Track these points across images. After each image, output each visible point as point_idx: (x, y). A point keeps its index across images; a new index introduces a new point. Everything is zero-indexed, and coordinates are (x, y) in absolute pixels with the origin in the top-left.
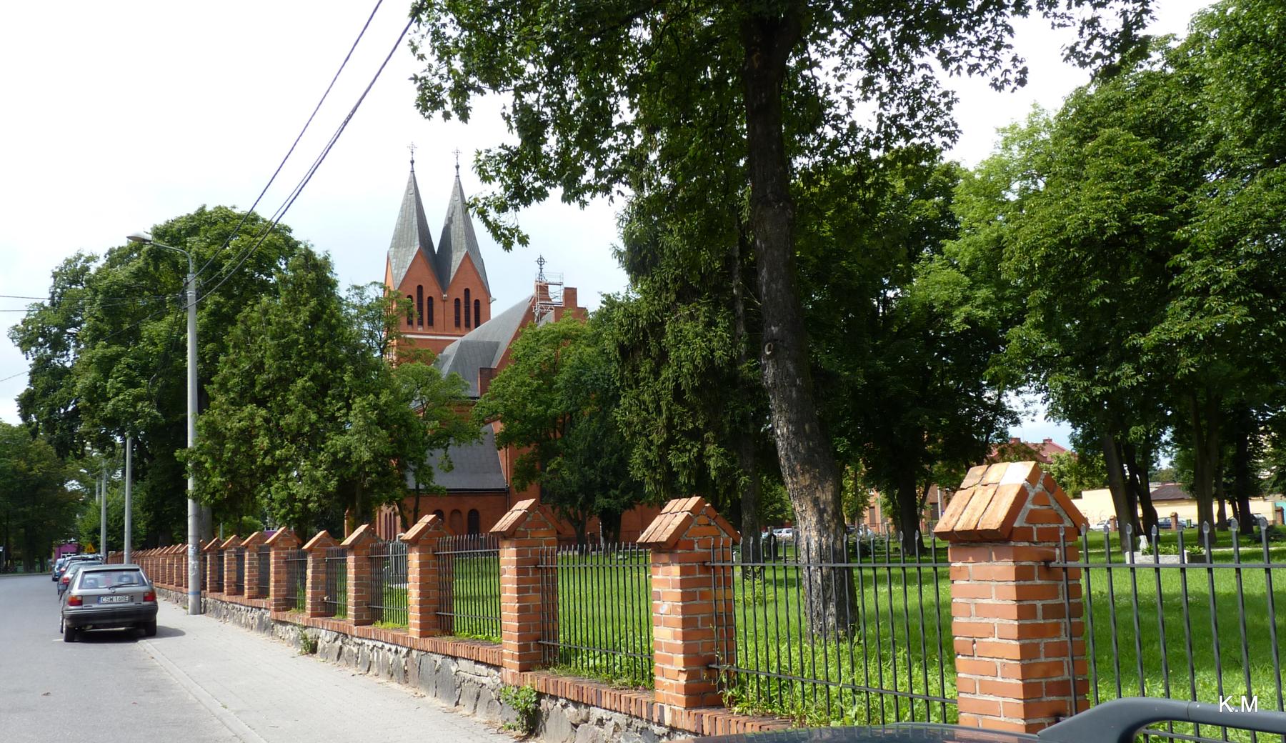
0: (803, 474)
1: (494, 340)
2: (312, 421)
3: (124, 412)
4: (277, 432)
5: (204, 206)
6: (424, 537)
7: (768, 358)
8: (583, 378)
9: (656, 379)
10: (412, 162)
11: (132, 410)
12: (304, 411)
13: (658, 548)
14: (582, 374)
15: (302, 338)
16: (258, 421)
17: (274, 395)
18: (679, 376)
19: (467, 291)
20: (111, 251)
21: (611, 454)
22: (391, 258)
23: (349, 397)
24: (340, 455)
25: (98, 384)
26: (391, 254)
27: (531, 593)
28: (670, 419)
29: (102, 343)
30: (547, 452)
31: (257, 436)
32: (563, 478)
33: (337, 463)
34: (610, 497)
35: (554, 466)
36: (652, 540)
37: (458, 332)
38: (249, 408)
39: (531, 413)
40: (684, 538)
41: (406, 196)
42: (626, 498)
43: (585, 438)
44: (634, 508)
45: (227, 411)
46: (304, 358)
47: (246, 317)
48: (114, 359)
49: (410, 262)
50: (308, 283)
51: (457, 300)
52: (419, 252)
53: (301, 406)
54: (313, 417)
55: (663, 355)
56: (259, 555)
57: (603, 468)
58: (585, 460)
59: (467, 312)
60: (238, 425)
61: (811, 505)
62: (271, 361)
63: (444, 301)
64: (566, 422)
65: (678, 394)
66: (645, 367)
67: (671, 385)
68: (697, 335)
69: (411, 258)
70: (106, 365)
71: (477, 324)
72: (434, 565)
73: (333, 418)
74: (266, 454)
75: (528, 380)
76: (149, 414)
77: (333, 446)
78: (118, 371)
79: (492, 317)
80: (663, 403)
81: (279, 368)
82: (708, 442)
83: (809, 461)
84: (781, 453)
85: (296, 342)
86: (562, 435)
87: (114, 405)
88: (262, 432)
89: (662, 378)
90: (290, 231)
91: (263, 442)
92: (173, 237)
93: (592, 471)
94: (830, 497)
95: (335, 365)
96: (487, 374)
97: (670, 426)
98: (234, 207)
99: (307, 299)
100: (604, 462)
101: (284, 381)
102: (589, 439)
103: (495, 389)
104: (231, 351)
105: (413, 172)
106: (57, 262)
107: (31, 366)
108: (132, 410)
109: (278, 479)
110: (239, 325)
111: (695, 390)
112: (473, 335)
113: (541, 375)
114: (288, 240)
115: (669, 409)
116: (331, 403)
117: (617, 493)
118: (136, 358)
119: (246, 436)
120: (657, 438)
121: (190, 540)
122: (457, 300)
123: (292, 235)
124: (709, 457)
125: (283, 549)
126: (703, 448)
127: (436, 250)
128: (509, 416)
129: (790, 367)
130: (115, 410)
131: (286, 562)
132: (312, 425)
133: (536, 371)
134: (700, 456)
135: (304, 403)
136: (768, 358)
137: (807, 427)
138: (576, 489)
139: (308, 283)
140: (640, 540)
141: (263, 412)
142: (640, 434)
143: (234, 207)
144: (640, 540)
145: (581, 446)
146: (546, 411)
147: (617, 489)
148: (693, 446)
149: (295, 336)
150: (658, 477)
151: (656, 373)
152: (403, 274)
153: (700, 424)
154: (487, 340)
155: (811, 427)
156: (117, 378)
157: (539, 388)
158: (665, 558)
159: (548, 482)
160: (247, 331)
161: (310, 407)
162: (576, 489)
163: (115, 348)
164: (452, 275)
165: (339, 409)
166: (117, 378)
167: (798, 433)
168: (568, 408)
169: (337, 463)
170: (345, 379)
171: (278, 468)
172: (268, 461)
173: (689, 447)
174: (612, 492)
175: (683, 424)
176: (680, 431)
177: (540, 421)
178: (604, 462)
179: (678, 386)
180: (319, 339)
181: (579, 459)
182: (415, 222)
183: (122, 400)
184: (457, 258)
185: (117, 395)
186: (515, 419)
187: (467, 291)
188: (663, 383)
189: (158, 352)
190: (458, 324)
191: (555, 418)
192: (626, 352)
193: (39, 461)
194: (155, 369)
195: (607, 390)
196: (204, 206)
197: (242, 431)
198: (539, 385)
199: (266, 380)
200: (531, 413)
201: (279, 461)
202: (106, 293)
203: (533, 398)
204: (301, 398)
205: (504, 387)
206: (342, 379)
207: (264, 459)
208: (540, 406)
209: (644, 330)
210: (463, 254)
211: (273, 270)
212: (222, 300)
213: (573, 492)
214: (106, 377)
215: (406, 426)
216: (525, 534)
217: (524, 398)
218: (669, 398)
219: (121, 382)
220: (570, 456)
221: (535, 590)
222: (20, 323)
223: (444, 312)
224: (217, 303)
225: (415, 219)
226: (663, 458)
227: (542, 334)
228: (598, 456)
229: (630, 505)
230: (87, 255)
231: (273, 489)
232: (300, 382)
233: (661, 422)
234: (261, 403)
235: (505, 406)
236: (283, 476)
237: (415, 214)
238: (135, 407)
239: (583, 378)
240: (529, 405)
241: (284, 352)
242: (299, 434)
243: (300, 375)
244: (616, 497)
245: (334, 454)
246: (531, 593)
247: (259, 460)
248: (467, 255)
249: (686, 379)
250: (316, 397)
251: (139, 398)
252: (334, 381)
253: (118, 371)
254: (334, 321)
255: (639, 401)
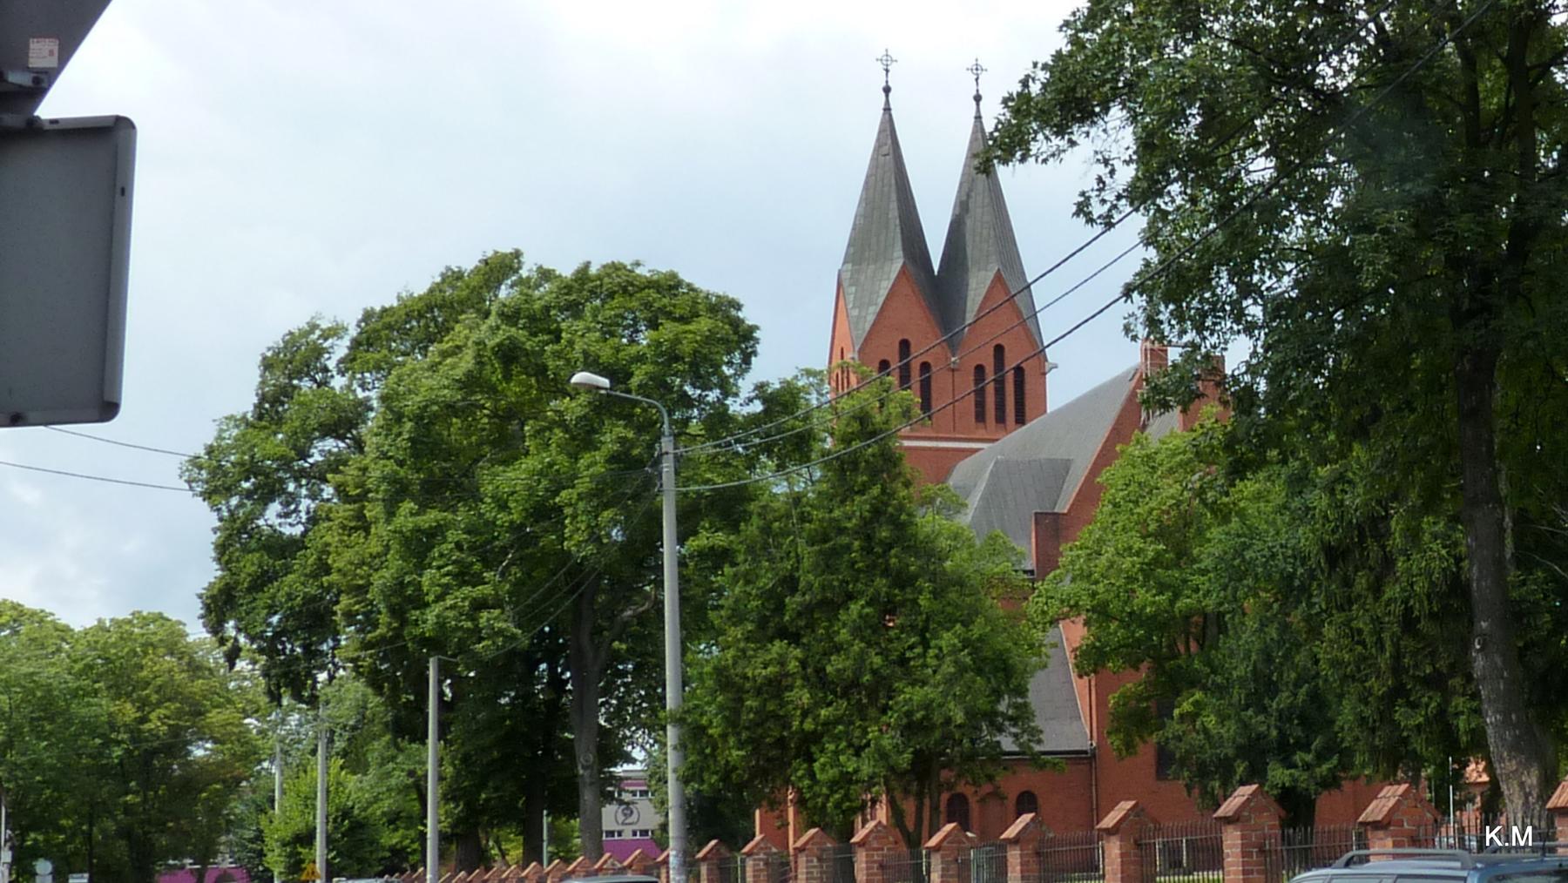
0: (1510, 760)
1: (1061, 454)
2: (875, 666)
3: (457, 628)
4: (819, 681)
5: (587, 265)
6: (1124, 825)
7: (1478, 651)
8: (1248, 555)
9: (1377, 599)
10: (887, 90)
11: (469, 624)
12: (862, 650)
13: (1377, 825)
14: (1246, 547)
15: (856, 544)
16: (793, 666)
17: (811, 627)
18: (1410, 597)
19: (999, 350)
20: (368, 316)
21: (1297, 685)
22: (845, 284)
23: (925, 629)
24: (919, 715)
25: (407, 579)
26: (846, 276)
27: (1255, 875)
28: (1397, 656)
29: (408, 506)
30: (1172, 682)
31: (790, 688)
32: (1206, 731)
33: (911, 728)
34: (1295, 766)
35: (1186, 707)
36: (1370, 819)
37: (981, 433)
38: (777, 647)
39: (1144, 607)
40: (1396, 817)
41: (874, 159)
42: (1325, 767)
43: (1248, 656)
44: (1339, 787)
45: (744, 651)
46: (859, 571)
47: (764, 507)
48: (435, 534)
49: (884, 293)
50: (867, 462)
51: (980, 370)
52: (903, 272)
53: (858, 646)
54: (877, 661)
55: (1388, 562)
56: (820, 860)
57: (1280, 712)
58: (1247, 696)
59: (1000, 384)
60: (764, 672)
61: (1517, 789)
62: (811, 577)
63: (953, 370)
64: (1211, 626)
65: (1408, 622)
66: (1361, 582)
67: (1397, 609)
68: (1435, 537)
69: (885, 287)
70: (419, 546)
71: (1021, 420)
72: (1135, 855)
73: (903, 661)
74: (805, 714)
75: (1138, 544)
76: (501, 632)
77: (906, 701)
78: (442, 555)
79: (1052, 406)
80: (1386, 636)
81: (823, 588)
82: (1454, 693)
83: (1515, 748)
84: (1491, 740)
85: (848, 548)
86: (1202, 646)
87: (438, 616)
88: (799, 682)
89: (1386, 596)
90: (738, 307)
91: (802, 696)
92: (532, 318)
93: (1261, 718)
94: (1535, 782)
95: (903, 580)
96: (1052, 528)
97: (1397, 669)
98: (638, 264)
99: (864, 484)
100: (1283, 700)
101: (830, 606)
102: (1254, 657)
103: (1072, 562)
104: (740, 558)
105: (887, 109)
106: (271, 336)
107: (215, 530)
108: (469, 624)
109: (822, 751)
110: (755, 519)
111: (1432, 616)
112: (1015, 441)
113: (1160, 535)
114: (736, 323)
115: (1396, 646)
116: (898, 638)
117: (1309, 758)
118: (468, 532)
119: (776, 687)
120: (1378, 687)
121: (672, 843)
122: (980, 370)
123: (741, 315)
124: (1457, 714)
125: (874, 849)
126: (1446, 701)
127: (936, 268)
128: (1101, 613)
129: (1498, 660)
130: (441, 624)
131: (882, 866)
132: (874, 672)
133: (1153, 527)
134: (1442, 712)
135: (862, 640)
136: (1478, 651)
137: (1514, 717)
138: (1231, 752)
139: (867, 462)
140: (1361, 819)
141: (798, 652)
142: (1353, 678)
143: (638, 264)
144: (1361, 819)
145: (1241, 670)
146: (1172, 602)
147: (1309, 752)
148: (1430, 698)
149: (845, 540)
150: (1377, 742)
151: (1377, 589)
152: (871, 318)
153: (1442, 665)
154: (1043, 456)
155: (1518, 717)
156: (439, 568)
157: (1157, 561)
158: (1381, 833)
159: (1180, 739)
160: (766, 530)
161: (869, 644)
162: (1231, 752)
163: (432, 517)
164: (970, 318)
165: (911, 648)
166: (439, 568)
167: (1506, 722)
168: (1221, 604)
169: (911, 728)
170: (922, 603)
171: (822, 736)
172: (809, 725)
173: (1425, 700)
174: (1299, 757)
175: (1416, 666)
176: (1413, 677)
177: (1158, 623)
178: (1283, 700)
179: (1408, 610)
180: (881, 542)
181: (1238, 694)
182: (894, 213)
183: (452, 607)
184: (978, 285)
185: (440, 598)
186: (1112, 618)
187: (999, 350)
188: (1388, 605)
189: (512, 522)
190: (980, 416)
191: (1187, 617)
192: (1334, 555)
193: (159, 704)
194: (504, 551)
195: (1292, 576)
196: (587, 265)
197: (769, 681)
198: (1158, 553)
199: (801, 604)
200: (1144, 607)
201: (825, 724)
202: (418, 419)
203: (1147, 577)
204: (857, 632)
205: (1089, 558)
206: (915, 602)
207: (802, 722)
208: (1161, 593)
209: (1359, 527)
210: (991, 275)
211: (714, 379)
212: (631, 435)
213: (1226, 757)
214: (421, 567)
215: (1004, 670)
216: (1249, 819)
217: (1131, 579)
218: (1396, 628)
219: (447, 574)
220: (1221, 690)
221: (1259, 872)
222: (202, 452)
223: (954, 389)
224: (622, 441)
225: (894, 205)
226: (1385, 716)
227: (1159, 458)
228: (1272, 689)
229: (1330, 782)
230: (325, 325)
231: (816, 765)
232: (854, 608)
233: (1384, 660)
234: (794, 638)
235: (1094, 595)
236: (831, 747)
237: (894, 197)
238: (474, 619)
239: (1248, 555)
240: (1141, 592)
241: (829, 560)
242: (855, 684)
243: (851, 597)
244: (1307, 767)
245: (909, 714)
246: (1255, 875)
247: (796, 723)
248: (998, 278)
249: (1421, 602)
250: (871, 630)
251: (479, 605)
252: (903, 604)
253: (442, 555)
254: (903, 517)
255: (1351, 629)
